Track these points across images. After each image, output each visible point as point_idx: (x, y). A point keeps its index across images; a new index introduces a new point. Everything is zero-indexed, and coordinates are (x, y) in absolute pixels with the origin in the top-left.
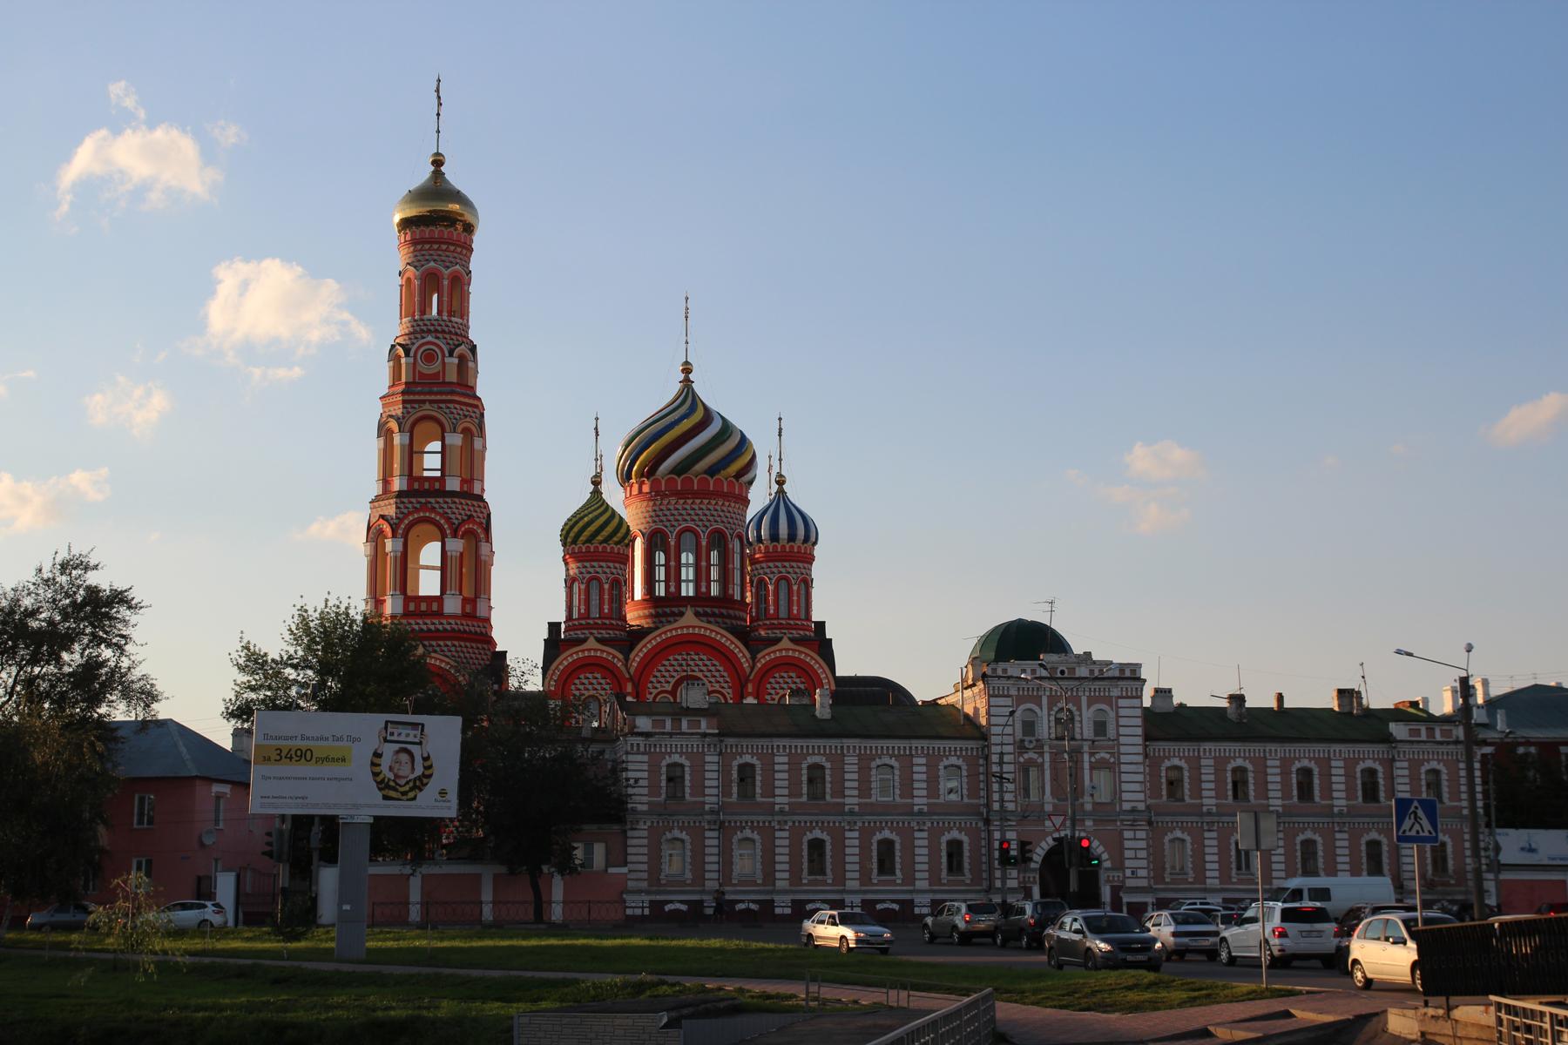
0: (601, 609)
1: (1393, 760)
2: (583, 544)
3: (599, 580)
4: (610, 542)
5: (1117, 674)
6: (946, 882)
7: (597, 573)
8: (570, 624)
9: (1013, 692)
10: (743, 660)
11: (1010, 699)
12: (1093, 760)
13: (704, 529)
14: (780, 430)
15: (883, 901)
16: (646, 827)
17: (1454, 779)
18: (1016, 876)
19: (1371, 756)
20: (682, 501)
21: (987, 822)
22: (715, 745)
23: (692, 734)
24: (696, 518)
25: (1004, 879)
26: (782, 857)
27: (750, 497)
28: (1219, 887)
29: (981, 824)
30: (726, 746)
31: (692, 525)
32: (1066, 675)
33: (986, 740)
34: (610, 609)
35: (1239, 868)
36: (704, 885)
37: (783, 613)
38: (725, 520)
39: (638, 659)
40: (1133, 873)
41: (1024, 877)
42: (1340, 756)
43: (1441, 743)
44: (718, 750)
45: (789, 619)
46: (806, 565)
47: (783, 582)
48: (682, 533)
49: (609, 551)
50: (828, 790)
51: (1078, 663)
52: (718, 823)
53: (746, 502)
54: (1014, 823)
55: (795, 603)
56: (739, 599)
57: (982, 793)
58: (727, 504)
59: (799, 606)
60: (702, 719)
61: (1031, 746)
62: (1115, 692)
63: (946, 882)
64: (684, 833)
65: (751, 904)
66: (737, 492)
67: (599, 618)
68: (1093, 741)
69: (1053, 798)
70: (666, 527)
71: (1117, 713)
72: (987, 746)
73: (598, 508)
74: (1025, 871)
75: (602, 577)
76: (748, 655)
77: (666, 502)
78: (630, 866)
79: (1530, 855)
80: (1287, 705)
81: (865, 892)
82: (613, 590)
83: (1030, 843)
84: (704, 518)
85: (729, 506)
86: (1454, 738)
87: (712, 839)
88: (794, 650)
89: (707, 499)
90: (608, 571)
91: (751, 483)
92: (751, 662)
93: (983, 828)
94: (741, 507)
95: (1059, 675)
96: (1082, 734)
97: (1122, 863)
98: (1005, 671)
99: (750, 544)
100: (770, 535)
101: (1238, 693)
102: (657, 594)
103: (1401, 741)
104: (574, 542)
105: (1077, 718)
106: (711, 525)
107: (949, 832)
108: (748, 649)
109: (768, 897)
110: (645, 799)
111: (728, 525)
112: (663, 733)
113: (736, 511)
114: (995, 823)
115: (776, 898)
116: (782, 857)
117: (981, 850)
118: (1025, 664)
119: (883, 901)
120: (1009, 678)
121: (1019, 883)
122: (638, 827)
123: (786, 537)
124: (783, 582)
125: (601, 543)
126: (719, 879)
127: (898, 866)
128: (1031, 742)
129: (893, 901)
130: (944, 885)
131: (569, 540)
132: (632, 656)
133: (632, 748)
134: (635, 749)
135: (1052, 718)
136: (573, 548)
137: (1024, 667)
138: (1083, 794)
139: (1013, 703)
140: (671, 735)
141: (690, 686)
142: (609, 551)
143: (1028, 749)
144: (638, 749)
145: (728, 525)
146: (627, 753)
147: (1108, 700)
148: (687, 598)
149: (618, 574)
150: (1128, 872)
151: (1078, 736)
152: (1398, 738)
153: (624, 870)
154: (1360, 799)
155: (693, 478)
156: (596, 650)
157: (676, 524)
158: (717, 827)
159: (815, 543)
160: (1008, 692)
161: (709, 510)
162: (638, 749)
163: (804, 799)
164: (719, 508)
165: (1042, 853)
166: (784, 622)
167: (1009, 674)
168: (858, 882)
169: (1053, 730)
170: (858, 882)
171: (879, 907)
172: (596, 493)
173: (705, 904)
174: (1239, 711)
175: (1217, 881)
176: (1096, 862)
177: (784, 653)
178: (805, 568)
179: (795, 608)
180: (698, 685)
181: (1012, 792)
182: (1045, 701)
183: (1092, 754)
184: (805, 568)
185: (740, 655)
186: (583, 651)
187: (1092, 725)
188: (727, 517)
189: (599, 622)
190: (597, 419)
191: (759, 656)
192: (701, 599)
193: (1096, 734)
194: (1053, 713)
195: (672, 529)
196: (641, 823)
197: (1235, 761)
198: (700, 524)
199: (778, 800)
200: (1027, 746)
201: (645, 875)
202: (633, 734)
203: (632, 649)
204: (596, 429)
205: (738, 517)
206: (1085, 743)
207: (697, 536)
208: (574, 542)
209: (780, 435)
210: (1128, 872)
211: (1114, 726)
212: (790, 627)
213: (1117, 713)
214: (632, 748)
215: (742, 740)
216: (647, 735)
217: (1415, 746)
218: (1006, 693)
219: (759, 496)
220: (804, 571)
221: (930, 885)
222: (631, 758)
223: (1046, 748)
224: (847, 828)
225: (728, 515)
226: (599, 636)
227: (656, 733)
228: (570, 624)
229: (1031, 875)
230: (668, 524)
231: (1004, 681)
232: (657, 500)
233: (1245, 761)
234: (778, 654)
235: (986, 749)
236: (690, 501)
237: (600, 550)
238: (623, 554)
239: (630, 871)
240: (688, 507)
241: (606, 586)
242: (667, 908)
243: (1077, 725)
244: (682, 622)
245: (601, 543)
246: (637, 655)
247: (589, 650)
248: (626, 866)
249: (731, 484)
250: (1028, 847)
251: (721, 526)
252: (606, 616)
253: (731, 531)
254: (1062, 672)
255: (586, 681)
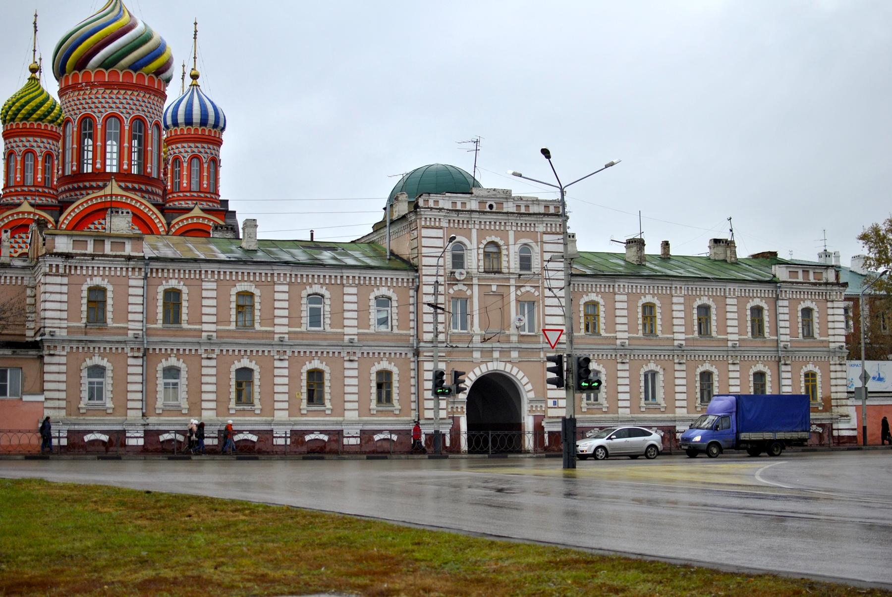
0: (35, 178)
1: (777, 299)
2: (21, 121)
3: (33, 152)
4: (44, 120)
5: (542, 210)
6: (375, 412)
7: (33, 146)
8: (8, 191)
9: (444, 224)
10: (159, 225)
11: (442, 230)
12: (519, 293)
13: (127, 116)
14: (196, 31)
15: (380, 432)
16: (65, 353)
17: (403, 380)
18: (445, 407)
19: (759, 295)
20: (108, 91)
21: (417, 353)
22: (140, 269)
23: (116, 256)
24: (121, 106)
25: (437, 409)
26: (209, 388)
27: (167, 93)
28: (630, 416)
29: (410, 355)
30: (152, 269)
31: (116, 111)
32: (494, 210)
33: (417, 271)
34: (44, 179)
35: (646, 398)
36: (126, 415)
37: (194, 187)
38: (145, 109)
39: (67, 222)
40: (555, 403)
41: (452, 408)
42: (734, 294)
43: (815, 284)
44: (143, 274)
45: (200, 192)
46: (215, 147)
47: (195, 161)
48: (110, 117)
49: (43, 128)
50: (257, 318)
51: (506, 198)
52: (142, 350)
53: (164, 97)
54: (444, 354)
55: (205, 178)
56: (156, 177)
57: (412, 324)
58: (147, 96)
59: (208, 180)
60: (127, 242)
61: (462, 278)
62: (541, 228)
63: (375, 412)
64: (106, 360)
65: (177, 435)
66: (156, 87)
67: (34, 186)
68: (520, 275)
69: (481, 330)
70: (94, 112)
71: (542, 248)
72: (419, 277)
73: (35, 91)
74: (454, 402)
75: (37, 150)
76: (164, 221)
77: (94, 91)
78: (48, 394)
79: (879, 383)
80: (673, 252)
81: (365, 423)
82: (45, 174)
83: (463, 373)
84: (127, 106)
85: (85, 94)
86: (824, 281)
87: (135, 368)
88: (204, 218)
89: (130, 90)
90: (42, 145)
91: (168, 81)
92: (166, 226)
93: (412, 359)
94: (160, 100)
95: (488, 210)
96: (509, 268)
97: (545, 394)
98: (436, 202)
99: (167, 127)
100: (185, 119)
101: (639, 237)
102: (85, 172)
103: (784, 282)
104: (12, 119)
105: (504, 252)
106: (133, 113)
107: (379, 363)
108: (164, 216)
109: (338, 428)
110: (64, 324)
111: (148, 114)
112: (85, 255)
113: (155, 103)
114: (425, 354)
115: (275, 428)
116: (209, 388)
117: (410, 381)
118: (457, 197)
119: (312, 432)
120: (441, 209)
121: (448, 413)
122: (57, 353)
123: (199, 121)
124: (195, 161)
125: (36, 120)
126: (142, 409)
127: (327, 396)
128: (461, 274)
129: (322, 432)
130: (373, 415)
131: (8, 118)
132: (61, 219)
133: (51, 270)
134: (54, 270)
135: (481, 251)
136: (12, 125)
137: (455, 200)
138: (509, 326)
139: (444, 234)
140: (93, 256)
141: (114, 213)
142: (43, 128)
143: (458, 280)
144: (57, 270)
145: (148, 114)
146: (45, 275)
147: (533, 235)
148: (111, 174)
149: (51, 149)
150: (550, 403)
151: (505, 270)
152: (781, 279)
153: (41, 398)
154: (750, 334)
155: (119, 72)
156: (29, 213)
157: (103, 110)
158: (141, 355)
159: (223, 129)
160: (439, 224)
161: (132, 99)
162: (57, 270)
163: (233, 327)
164: (140, 99)
165: (474, 378)
166: (195, 194)
167: (440, 206)
168: (287, 413)
169: (481, 263)
170: (287, 413)
171: (377, 437)
172: (34, 81)
173: (128, 435)
174: (639, 254)
175: (628, 410)
176: (583, 384)
177: (195, 221)
178: (214, 149)
179: (205, 182)
180: (122, 213)
181: (442, 323)
182: (474, 233)
183: (518, 287)
184: (214, 149)
185: (157, 221)
186: (18, 213)
187: (518, 259)
188: (147, 107)
189: (33, 189)
190: (36, 16)
191: (174, 222)
192: (122, 176)
193: (522, 268)
194: (482, 246)
195: (99, 115)
196: (59, 348)
197: (645, 297)
198: (124, 111)
199: (205, 327)
200: (459, 278)
201: (63, 404)
202: (52, 254)
203: (61, 214)
204: (35, 23)
205: (157, 108)
206: (512, 276)
207: (121, 121)
208: (12, 119)
209: (195, 38)
210: (550, 403)
211: (539, 261)
212: (200, 199)
213: (542, 248)
214: (51, 270)
215: (168, 264)
216: (68, 256)
217: (795, 286)
218: (437, 224)
219: (174, 92)
220: (213, 152)
221: (359, 416)
222: (49, 279)
223: (475, 281)
224: (277, 357)
225: (148, 105)
226: (33, 202)
227: (77, 255)
228: (8, 191)
229: (459, 406)
230: (96, 110)
231: (435, 213)
232: (87, 89)
233: (653, 297)
234: (190, 221)
235: (417, 280)
236: (115, 92)
237: (35, 127)
238: (56, 132)
239: (46, 399)
240: (114, 96)
241: (40, 159)
242: (87, 438)
243: (504, 258)
244: (107, 191)
245: (36, 120)
246: (66, 218)
247: (23, 213)
248: (43, 394)
249: (151, 79)
250: (461, 378)
251: (142, 114)
252: (39, 185)
253: (151, 120)
254: (491, 206)
255: (20, 241)
